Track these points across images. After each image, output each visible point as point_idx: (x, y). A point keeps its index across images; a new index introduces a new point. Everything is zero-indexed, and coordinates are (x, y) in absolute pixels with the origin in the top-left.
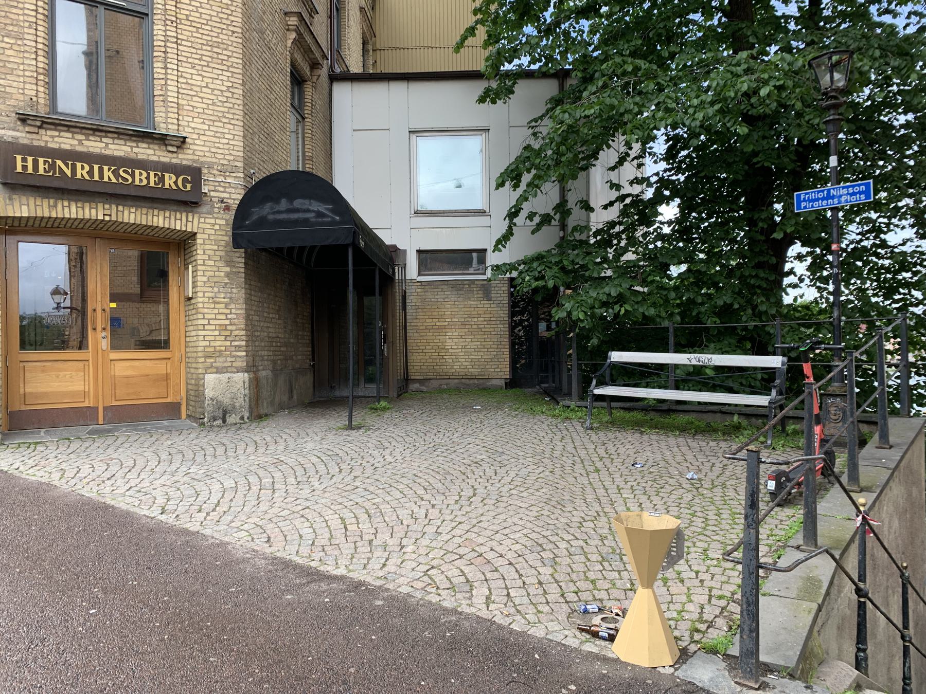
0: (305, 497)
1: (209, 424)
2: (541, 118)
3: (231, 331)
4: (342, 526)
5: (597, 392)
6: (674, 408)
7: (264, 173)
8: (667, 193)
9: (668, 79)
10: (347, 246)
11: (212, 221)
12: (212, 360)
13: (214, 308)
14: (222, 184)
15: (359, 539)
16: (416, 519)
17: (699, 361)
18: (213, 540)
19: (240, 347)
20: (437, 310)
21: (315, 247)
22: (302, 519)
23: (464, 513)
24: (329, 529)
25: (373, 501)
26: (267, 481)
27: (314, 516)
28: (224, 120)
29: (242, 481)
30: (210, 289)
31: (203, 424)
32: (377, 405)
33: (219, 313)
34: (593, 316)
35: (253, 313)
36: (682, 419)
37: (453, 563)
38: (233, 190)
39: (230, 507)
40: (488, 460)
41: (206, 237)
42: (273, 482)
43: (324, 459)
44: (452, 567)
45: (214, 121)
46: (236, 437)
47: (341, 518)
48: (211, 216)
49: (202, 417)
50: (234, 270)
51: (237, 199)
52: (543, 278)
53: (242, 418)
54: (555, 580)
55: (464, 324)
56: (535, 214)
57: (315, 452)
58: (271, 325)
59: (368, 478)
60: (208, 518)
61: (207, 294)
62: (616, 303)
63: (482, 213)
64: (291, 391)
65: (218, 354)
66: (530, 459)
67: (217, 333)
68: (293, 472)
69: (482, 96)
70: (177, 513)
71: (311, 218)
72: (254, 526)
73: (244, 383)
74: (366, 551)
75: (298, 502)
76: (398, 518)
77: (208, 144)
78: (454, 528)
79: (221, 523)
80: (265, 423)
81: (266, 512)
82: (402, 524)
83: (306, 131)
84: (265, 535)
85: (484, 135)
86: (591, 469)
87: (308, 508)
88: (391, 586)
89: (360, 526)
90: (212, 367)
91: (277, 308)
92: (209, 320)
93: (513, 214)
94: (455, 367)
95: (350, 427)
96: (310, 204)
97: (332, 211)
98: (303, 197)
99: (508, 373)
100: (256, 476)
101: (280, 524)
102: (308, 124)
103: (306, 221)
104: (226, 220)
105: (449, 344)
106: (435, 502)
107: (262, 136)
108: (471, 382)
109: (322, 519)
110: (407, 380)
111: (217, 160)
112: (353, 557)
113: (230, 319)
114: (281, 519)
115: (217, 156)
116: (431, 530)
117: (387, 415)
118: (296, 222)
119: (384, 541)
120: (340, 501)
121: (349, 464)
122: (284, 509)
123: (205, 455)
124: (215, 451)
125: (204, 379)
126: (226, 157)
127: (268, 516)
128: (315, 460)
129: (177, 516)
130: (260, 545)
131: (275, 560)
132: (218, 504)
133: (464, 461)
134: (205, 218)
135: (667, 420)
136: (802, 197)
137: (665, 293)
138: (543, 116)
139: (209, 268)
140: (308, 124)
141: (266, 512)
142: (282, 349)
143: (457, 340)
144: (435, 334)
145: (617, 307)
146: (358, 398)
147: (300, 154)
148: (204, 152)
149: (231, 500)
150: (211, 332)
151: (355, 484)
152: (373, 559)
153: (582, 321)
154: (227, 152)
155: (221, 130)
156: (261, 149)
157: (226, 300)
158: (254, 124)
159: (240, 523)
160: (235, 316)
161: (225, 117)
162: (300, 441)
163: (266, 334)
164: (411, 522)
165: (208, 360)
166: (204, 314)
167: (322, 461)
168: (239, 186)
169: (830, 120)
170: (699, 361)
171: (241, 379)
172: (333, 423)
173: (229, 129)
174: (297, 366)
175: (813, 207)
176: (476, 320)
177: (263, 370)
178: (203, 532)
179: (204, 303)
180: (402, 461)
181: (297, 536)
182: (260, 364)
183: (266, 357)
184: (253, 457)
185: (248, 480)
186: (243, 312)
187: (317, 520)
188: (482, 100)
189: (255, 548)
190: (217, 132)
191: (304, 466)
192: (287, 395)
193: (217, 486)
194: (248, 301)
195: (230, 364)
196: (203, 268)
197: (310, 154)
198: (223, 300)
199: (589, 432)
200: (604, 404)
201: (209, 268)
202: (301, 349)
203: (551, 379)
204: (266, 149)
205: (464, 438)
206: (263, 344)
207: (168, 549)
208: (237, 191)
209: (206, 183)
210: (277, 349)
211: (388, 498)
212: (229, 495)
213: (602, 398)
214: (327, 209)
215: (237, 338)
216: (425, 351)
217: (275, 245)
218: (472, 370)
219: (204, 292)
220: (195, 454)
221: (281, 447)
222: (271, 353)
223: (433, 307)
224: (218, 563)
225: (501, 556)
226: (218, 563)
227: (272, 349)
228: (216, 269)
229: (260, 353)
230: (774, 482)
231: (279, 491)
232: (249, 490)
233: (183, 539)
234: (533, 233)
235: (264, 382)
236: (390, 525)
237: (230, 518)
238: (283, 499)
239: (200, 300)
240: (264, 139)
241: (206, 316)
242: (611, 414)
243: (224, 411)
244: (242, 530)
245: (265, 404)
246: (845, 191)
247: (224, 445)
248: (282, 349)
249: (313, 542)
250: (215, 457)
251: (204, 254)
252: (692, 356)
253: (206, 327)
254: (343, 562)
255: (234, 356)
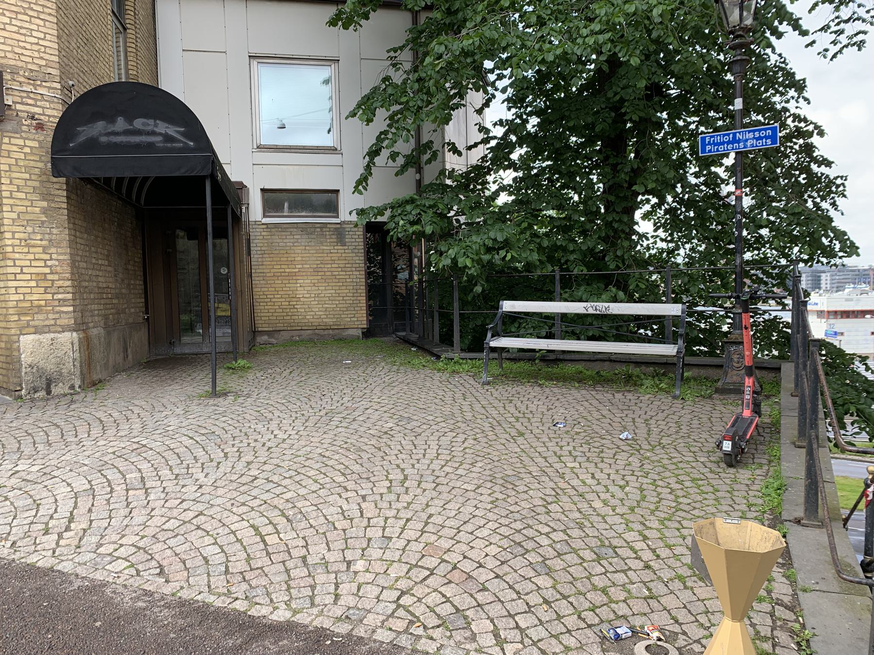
0: (192, 497)
1: (28, 397)
2: (401, 48)
3: (53, 281)
4: (258, 539)
5: (493, 344)
6: (561, 357)
7: (85, 87)
8: (513, 138)
9: (549, 12)
10: (204, 178)
11: (21, 142)
12: (29, 318)
13: (28, 253)
14: (32, 95)
15: (287, 557)
16: (352, 520)
17: (596, 310)
18: (77, 583)
19: (64, 300)
20: (286, 255)
21: (149, 177)
22: (199, 531)
23: (405, 505)
24: (242, 544)
25: (285, 496)
26: (133, 476)
27: (215, 525)
28: (31, 13)
29: (97, 479)
30: (22, 229)
31: (21, 397)
32: (234, 364)
33: (35, 259)
34: (479, 261)
35: (79, 258)
36: (570, 368)
37: (426, 582)
38: (47, 105)
39: (91, 521)
40: (398, 428)
41: (13, 161)
42: (142, 478)
43: (198, 439)
44: (427, 590)
45: (17, 13)
46: (71, 413)
47: (252, 526)
48: (18, 136)
49: (18, 388)
50: (53, 205)
51: (54, 116)
52: (417, 222)
53: (72, 387)
54: (561, 594)
55: (316, 271)
56: (398, 154)
57: (183, 431)
58: (101, 274)
59: (265, 463)
60: (62, 542)
61: (17, 236)
62: (502, 248)
63: (332, 150)
64: (125, 350)
65: (36, 310)
66: (443, 424)
67: (33, 284)
68: (163, 460)
69: (333, 19)
70: (12, 538)
71: (158, 142)
72: (134, 550)
73: (72, 344)
74: (303, 575)
75: (185, 505)
76: (327, 519)
77: (9, 42)
78: (403, 529)
79: (83, 549)
80: (103, 393)
81: (145, 525)
82: (335, 528)
83: (128, 44)
84: (154, 563)
85: (333, 66)
86: (514, 433)
87: (201, 513)
88: (360, 632)
89: (281, 535)
90: (28, 326)
91: (106, 252)
92: (22, 267)
93: (374, 153)
94: (308, 317)
95: (215, 393)
96: (156, 125)
97: (183, 134)
98: (146, 116)
99: (365, 322)
100: (115, 470)
101: (172, 542)
102: (131, 36)
103: (151, 146)
104: (39, 141)
105: (301, 292)
106: (364, 493)
107: (80, 40)
108: (326, 332)
109: (227, 531)
110: (255, 333)
111: (23, 64)
112: (289, 588)
113: (51, 267)
114: (170, 534)
115: (23, 58)
116: (375, 533)
117: (250, 376)
118: (137, 147)
119: (321, 556)
120: (241, 499)
121: (233, 445)
122: (170, 519)
123: (34, 443)
124: (48, 436)
125: (19, 341)
126: (35, 61)
127: (149, 532)
128: (188, 442)
129: (14, 543)
130: (154, 583)
131: (185, 607)
132: (71, 519)
133: (371, 432)
134: (10, 137)
135: (555, 370)
136: (707, 140)
137: (538, 240)
138: (403, 46)
139: (18, 202)
140: (131, 36)
141: (145, 525)
142: (115, 301)
143: (309, 288)
144: (284, 282)
145: (502, 253)
146: (203, 354)
147: (123, 71)
148: (5, 51)
149: (90, 511)
150: (26, 282)
151: (252, 473)
152: (318, 587)
153: (470, 269)
154: (36, 54)
155: (27, 25)
156: (79, 56)
157: (44, 243)
158: (70, 23)
159: (112, 547)
160: (57, 263)
161: (32, 9)
162: (158, 416)
163: (95, 284)
164: (346, 524)
165: (22, 318)
166: (14, 260)
167: (197, 442)
168: (56, 100)
169: (737, 60)
170: (596, 310)
171: (68, 340)
172: (189, 390)
173: (38, 26)
174: (131, 320)
175: (718, 150)
176: (329, 266)
177: (94, 327)
178: (59, 567)
179: (13, 246)
180: (297, 437)
181: (199, 561)
182: (90, 320)
183: (96, 312)
184: (103, 443)
185: (105, 476)
186: (67, 257)
187: (220, 531)
188: (333, 23)
189: (146, 587)
190: (21, 27)
191: (176, 451)
192: (122, 355)
193: (63, 490)
194: (72, 243)
195: (52, 322)
196: (11, 201)
197: (135, 73)
198: (39, 242)
199: (486, 387)
200: (496, 355)
201: (18, 202)
202: (133, 301)
203: (408, 329)
204: (85, 58)
205: (356, 402)
206: (92, 296)
207: (13, 607)
208: (52, 106)
209: (10, 92)
210: (108, 301)
211: (302, 492)
212: (84, 504)
213: (494, 350)
214: (178, 132)
215: (61, 290)
216: (274, 300)
217: (101, 174)
218: (327, 320)
219: (14, 233)
220: (19, 441)
221: (137, 426)
222: (102, 307)
223: (282, 252)
224: (98, 624)
225: (481, 566)
226: (98, 624)
227: (102, 302)
228: (29, 204)
229: (89, 307)
230: (730, 443)
231: (154, 491)
232: (111, 492)
233: (32, 584)
234: (397, 174)
235: (96, 341)
236: (321, 531)
237: (95, 539)
238: (163, 502)
239: (9, 242)
240: (83, 44)
241: (18, 263)
242: (501, 366)
243: (47, 379)
244: (118, 558)
245: (98, 368)
246: (751, 135)
247: (58, 427)
248: (115, 301)
249: (227, 567)
250: (50, 445)
251: (11, 183)
252: (588, 304)
253: (19, 277)
254: (280, 597)
255: (57, 313)
